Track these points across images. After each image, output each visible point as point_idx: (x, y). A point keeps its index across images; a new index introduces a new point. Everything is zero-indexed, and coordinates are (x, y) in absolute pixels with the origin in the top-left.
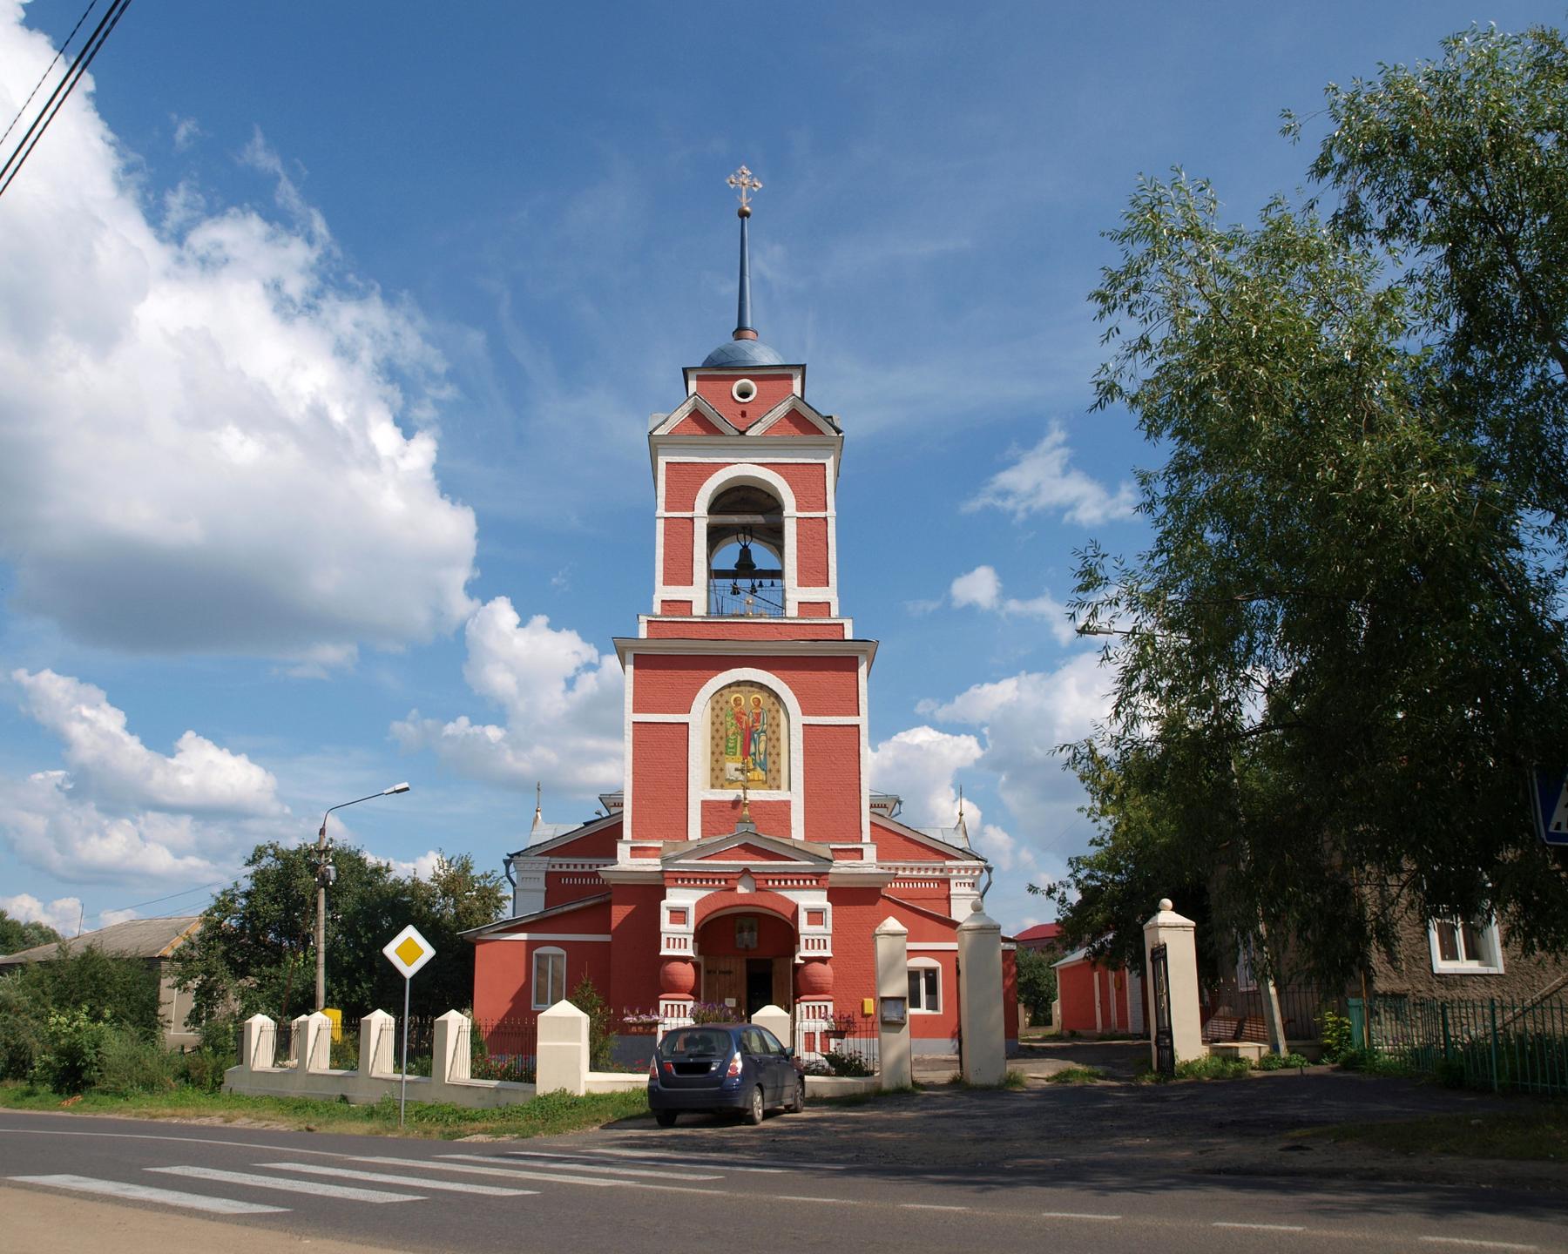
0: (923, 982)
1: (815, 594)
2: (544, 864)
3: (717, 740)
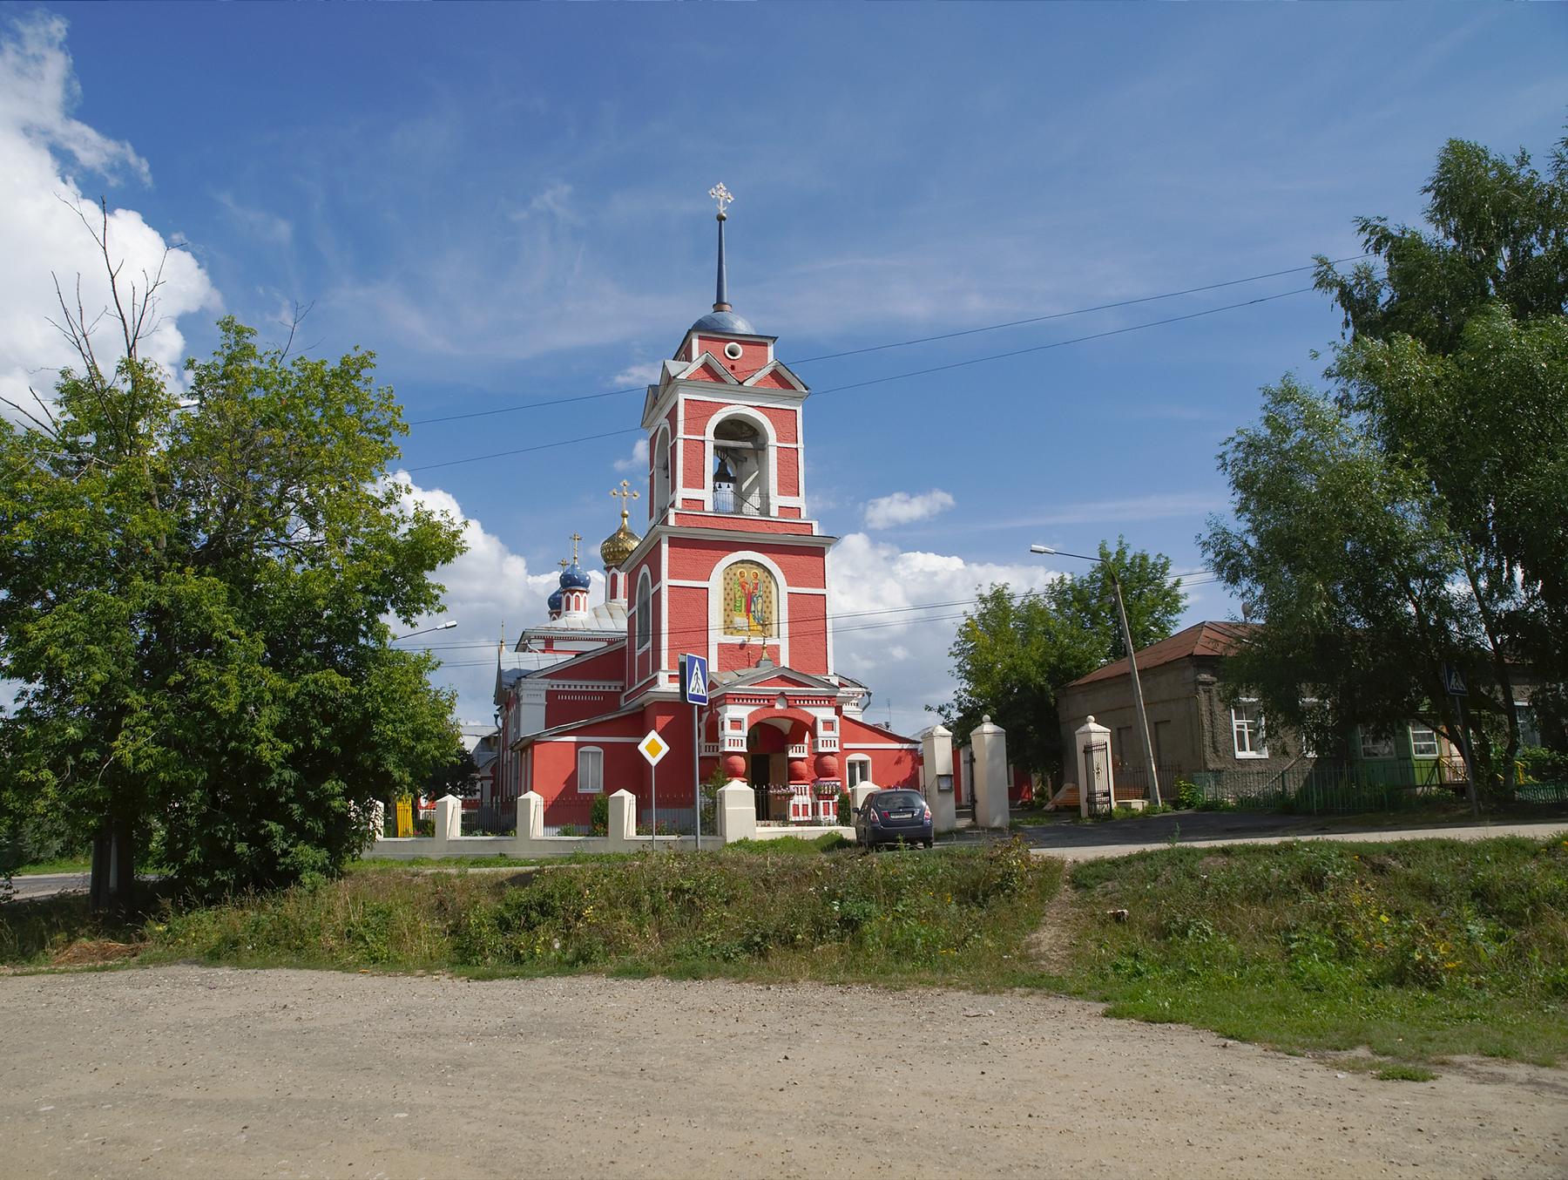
1: (790, 501)
2: (546, 684)
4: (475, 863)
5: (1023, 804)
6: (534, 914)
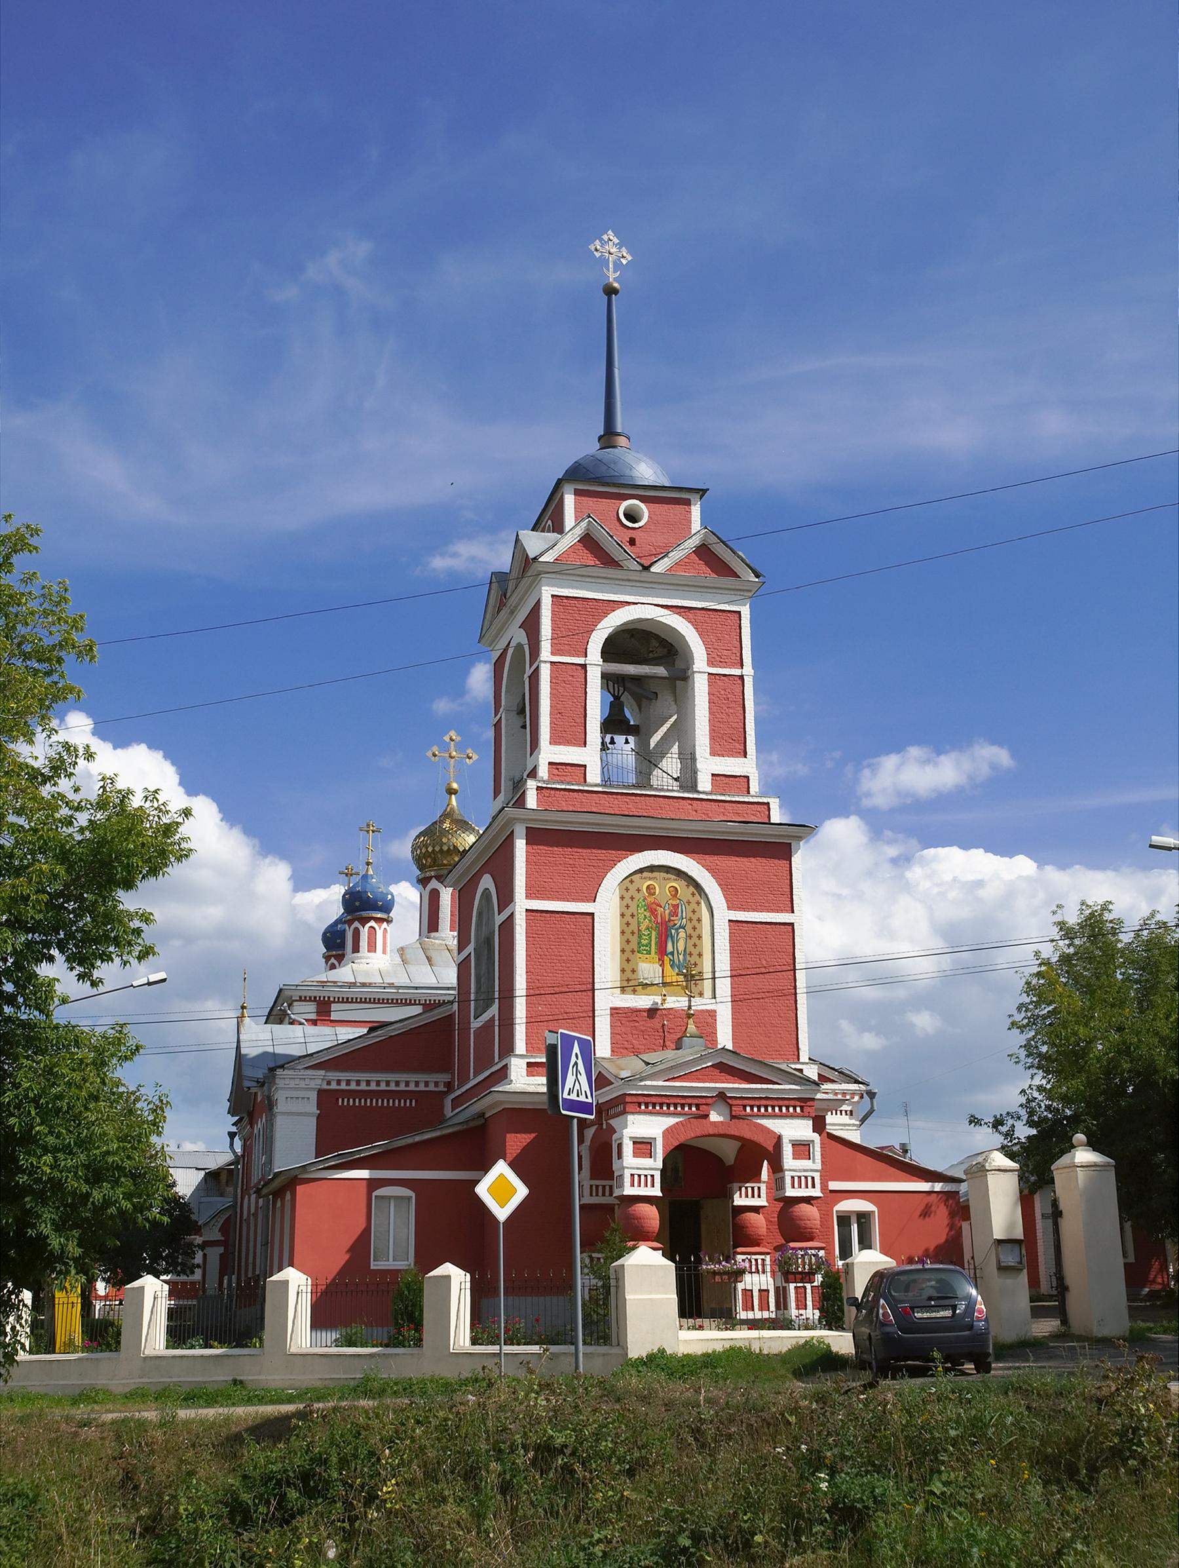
0: (855, 1228)
1: (731, 766)
2: (319, 1079)
3: (628, 935)
4: (192, 1398)
5: (1153, 1295)
6: (293, 1494)
